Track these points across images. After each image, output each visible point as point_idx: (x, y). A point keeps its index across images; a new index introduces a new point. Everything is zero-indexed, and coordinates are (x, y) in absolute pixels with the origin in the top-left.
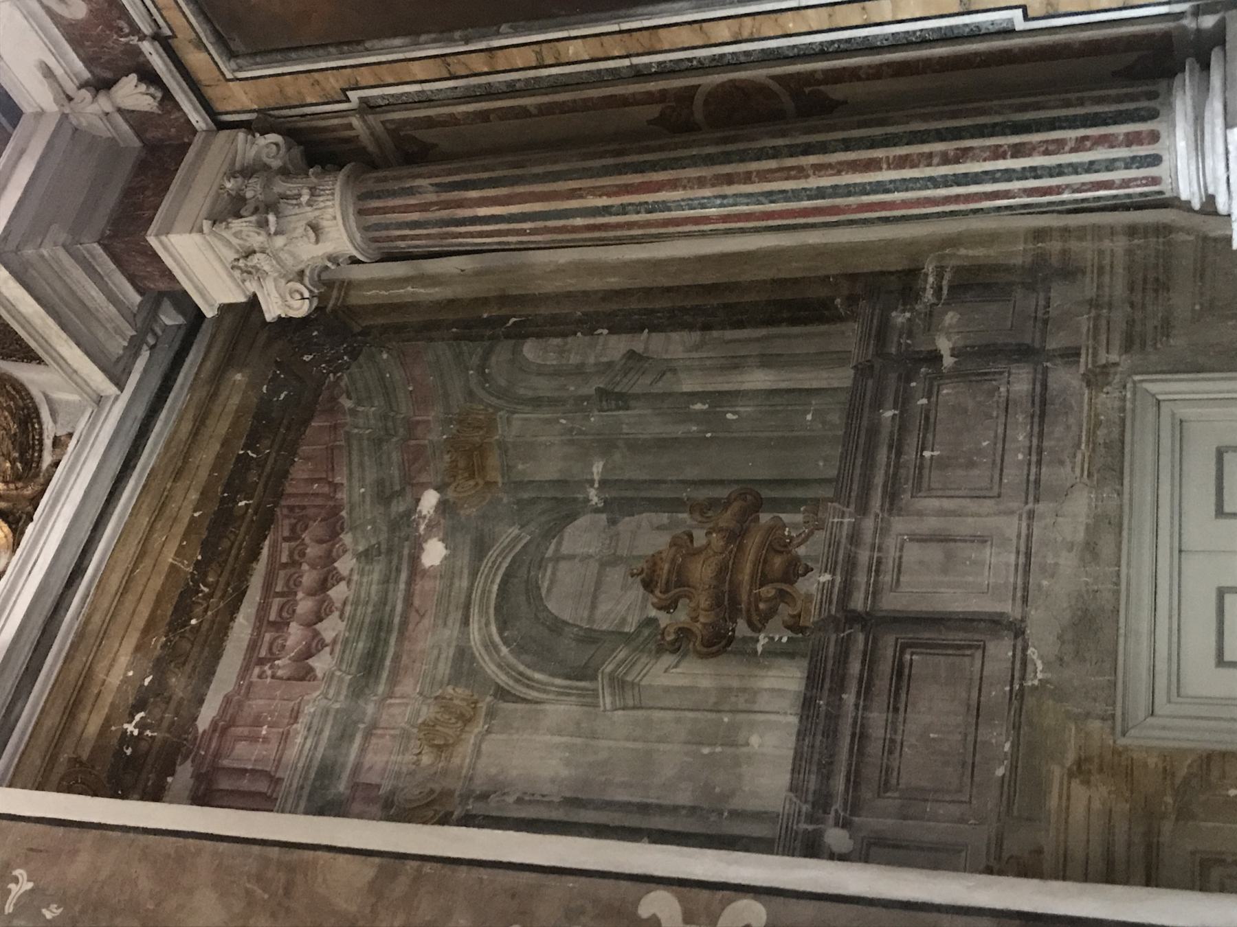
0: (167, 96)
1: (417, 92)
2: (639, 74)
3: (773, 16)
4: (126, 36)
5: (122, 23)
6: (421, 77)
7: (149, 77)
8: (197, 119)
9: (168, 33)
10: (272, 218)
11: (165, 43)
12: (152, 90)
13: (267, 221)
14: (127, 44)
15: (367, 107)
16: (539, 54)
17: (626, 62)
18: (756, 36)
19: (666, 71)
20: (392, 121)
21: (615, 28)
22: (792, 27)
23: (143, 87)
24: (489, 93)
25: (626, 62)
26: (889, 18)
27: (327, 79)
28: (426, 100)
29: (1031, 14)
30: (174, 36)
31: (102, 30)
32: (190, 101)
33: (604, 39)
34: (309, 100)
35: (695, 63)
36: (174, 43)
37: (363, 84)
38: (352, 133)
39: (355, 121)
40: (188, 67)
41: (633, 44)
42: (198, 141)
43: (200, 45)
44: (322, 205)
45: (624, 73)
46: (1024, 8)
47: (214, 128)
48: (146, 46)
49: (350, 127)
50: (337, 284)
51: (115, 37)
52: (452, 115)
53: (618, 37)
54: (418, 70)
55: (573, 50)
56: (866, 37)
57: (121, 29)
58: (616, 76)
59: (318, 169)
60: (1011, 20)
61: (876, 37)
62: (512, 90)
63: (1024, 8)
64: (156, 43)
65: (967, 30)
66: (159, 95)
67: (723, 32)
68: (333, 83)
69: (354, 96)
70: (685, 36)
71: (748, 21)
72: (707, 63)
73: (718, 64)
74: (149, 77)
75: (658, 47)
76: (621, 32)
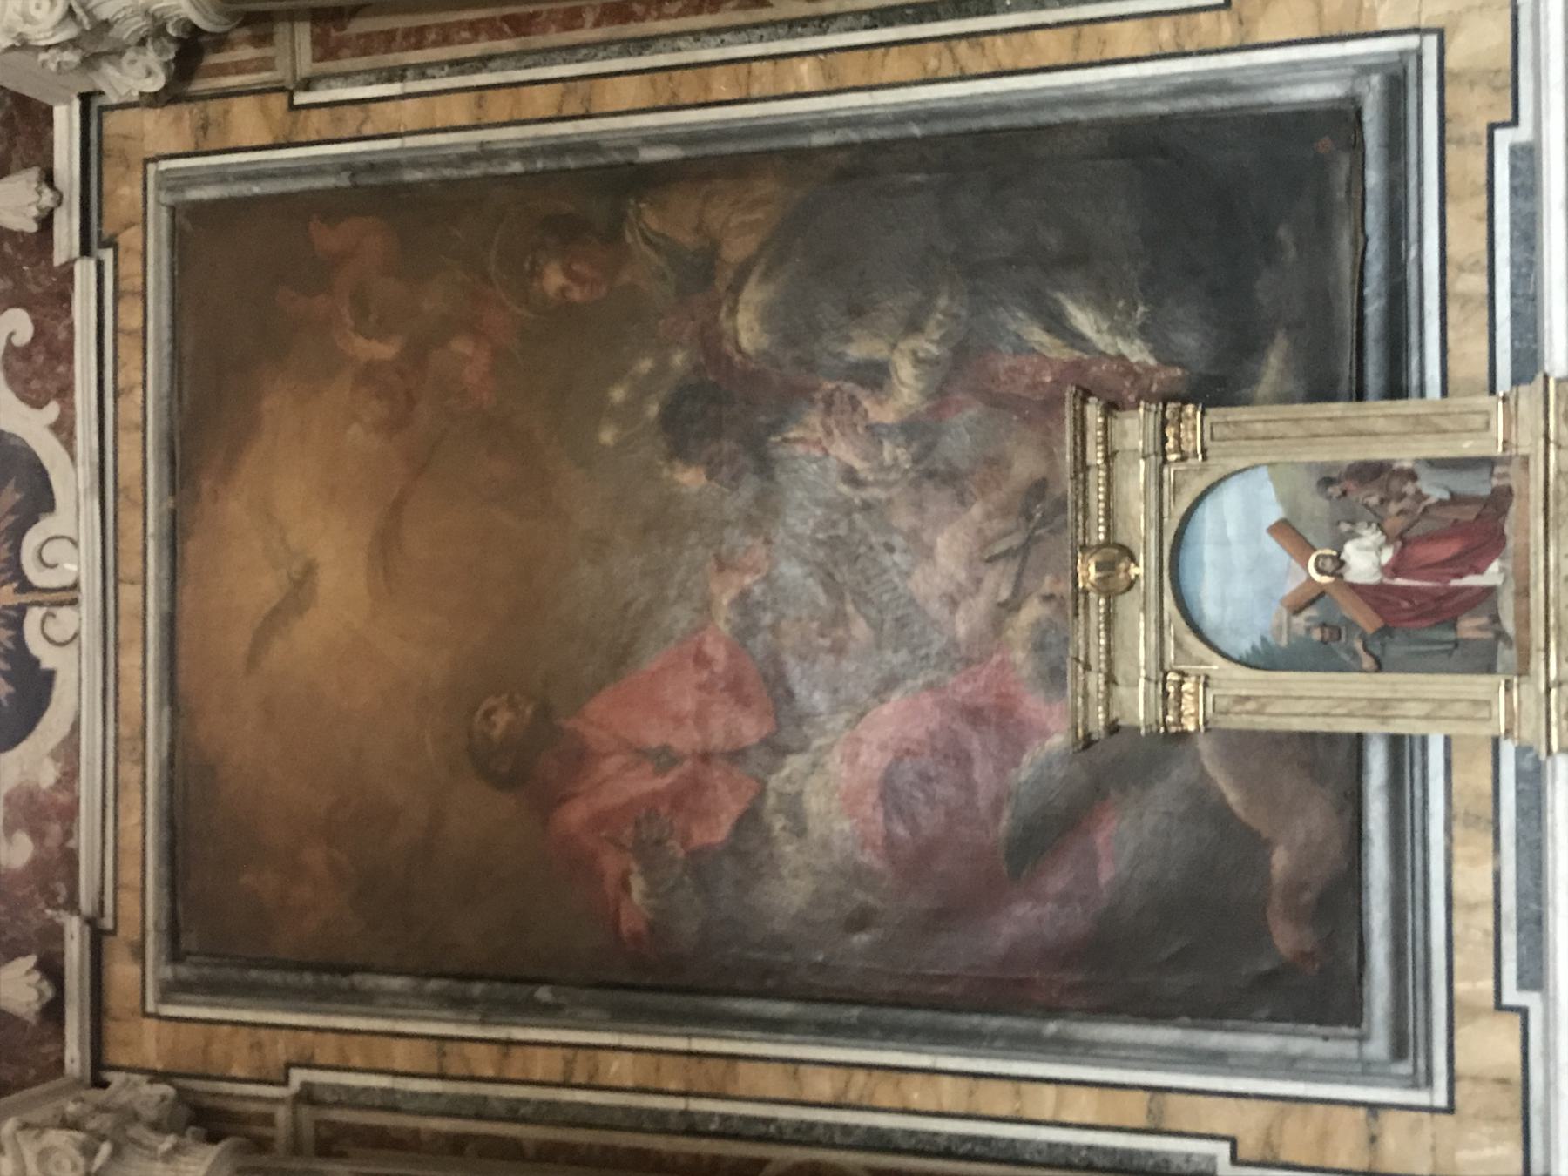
0: (53, 1011)
1: (384, 1091)
2: (692, 1126)
3: (895, 1075)
4: (56, 907)
5: (62, 889)
6: (399, 1065)
7: (52, 969)
8: (74, 1054)
9: (108, 923)
10: (105, 1149)
11: (98, 938)
12: (45, 985)
13: (95, 1152)
14: (51, 920)
15: (307, 1096)
16: (569, 1063)
17: (679, 1104)
18: (865, 1102)
19: (732, 1130)
20: (331, 1124)
21: (680, 1044)
22: (916, 1099)
23: (37, 976)
24: (480, 1109)
25: (679, 1104)
26: (1047, 1115)
27: (275, 1042)
28: (389, 1102)
29: (1243, 1154)
30: (114, 932)
31: (32, 893)
32: (81, 1027)
33: (665, 1059)
34: (236, 1071)
35: (772, 1129)
36: (107, 940)
37: (320, 1060)
38: (267, 1132)
39: (282, 1114)
40: (104, 978)
41: (702, 1075)
42: (60, 1082)
43: (139, 952)
44: (182, 1167)
45: (673, 1122)
46: (1233, 1142)
47: (88, 1081)
48: (73, 927)
49: (268, 1120)
50: (399, 34)
51: (42, 905)
52: (416, 1133)
53: (684, 1060)
54: (401, 1054)
55: (618, 1068)
56: (1012, 1141)
57: (55, 895)
58: (659, 1122)
59: (201, 1131)
60: (1212, 1159)
61: (1027, 1143)
62: (514, 1112)
63: (1233, 1142)
64: (87, 928)
65: (1151, 1162)
66: (49, 993)
67: (822, 1085)
68: (281, 1049)
69: (298, 1076)
70: (772, 1081)
71: (860, 1077)
72: (788, 1133)
73: (805, 1135)
74: (52, 969)
75: (730, 1091)
76: (689, 1053)
